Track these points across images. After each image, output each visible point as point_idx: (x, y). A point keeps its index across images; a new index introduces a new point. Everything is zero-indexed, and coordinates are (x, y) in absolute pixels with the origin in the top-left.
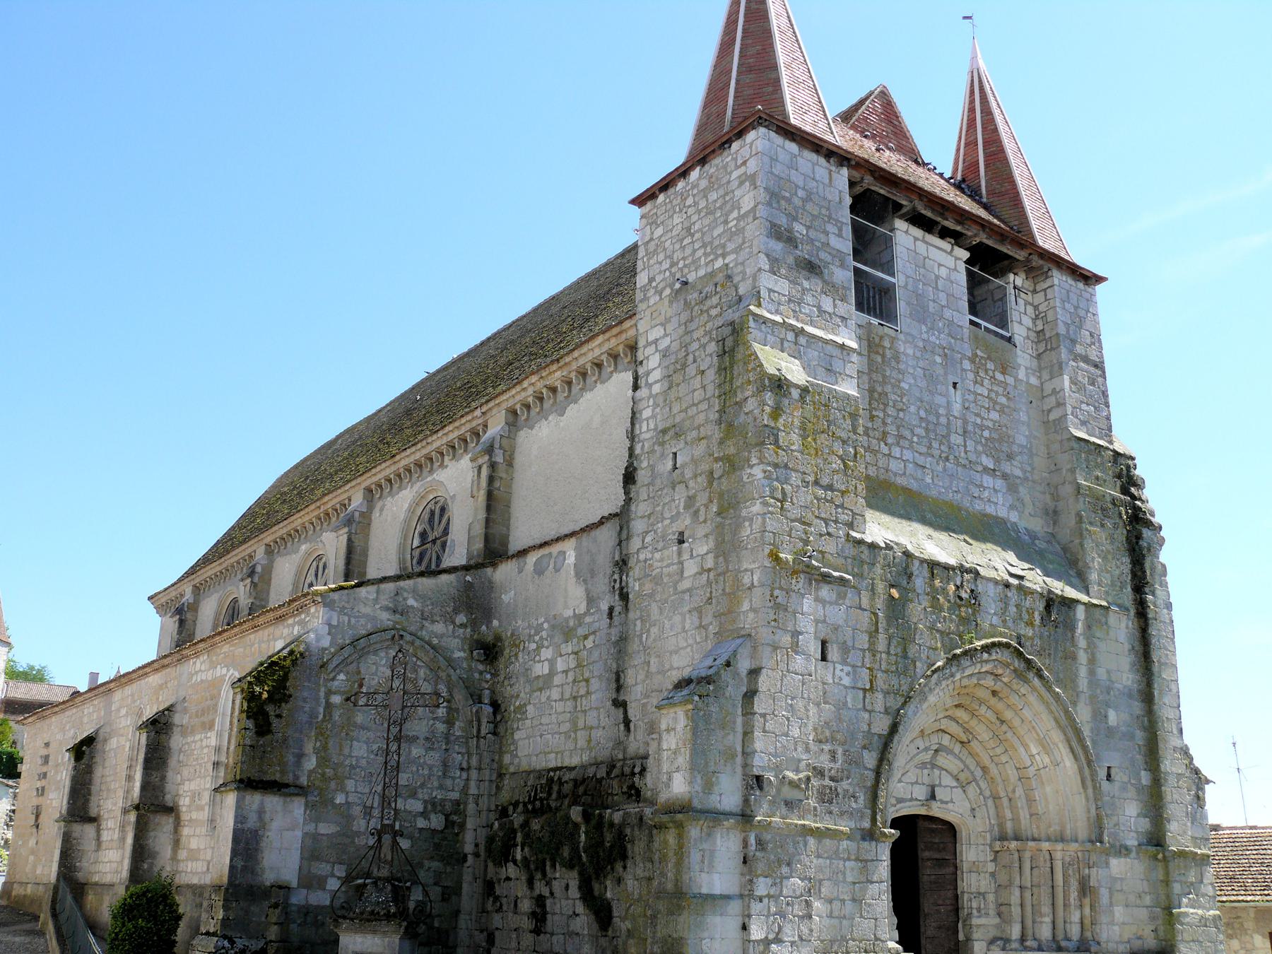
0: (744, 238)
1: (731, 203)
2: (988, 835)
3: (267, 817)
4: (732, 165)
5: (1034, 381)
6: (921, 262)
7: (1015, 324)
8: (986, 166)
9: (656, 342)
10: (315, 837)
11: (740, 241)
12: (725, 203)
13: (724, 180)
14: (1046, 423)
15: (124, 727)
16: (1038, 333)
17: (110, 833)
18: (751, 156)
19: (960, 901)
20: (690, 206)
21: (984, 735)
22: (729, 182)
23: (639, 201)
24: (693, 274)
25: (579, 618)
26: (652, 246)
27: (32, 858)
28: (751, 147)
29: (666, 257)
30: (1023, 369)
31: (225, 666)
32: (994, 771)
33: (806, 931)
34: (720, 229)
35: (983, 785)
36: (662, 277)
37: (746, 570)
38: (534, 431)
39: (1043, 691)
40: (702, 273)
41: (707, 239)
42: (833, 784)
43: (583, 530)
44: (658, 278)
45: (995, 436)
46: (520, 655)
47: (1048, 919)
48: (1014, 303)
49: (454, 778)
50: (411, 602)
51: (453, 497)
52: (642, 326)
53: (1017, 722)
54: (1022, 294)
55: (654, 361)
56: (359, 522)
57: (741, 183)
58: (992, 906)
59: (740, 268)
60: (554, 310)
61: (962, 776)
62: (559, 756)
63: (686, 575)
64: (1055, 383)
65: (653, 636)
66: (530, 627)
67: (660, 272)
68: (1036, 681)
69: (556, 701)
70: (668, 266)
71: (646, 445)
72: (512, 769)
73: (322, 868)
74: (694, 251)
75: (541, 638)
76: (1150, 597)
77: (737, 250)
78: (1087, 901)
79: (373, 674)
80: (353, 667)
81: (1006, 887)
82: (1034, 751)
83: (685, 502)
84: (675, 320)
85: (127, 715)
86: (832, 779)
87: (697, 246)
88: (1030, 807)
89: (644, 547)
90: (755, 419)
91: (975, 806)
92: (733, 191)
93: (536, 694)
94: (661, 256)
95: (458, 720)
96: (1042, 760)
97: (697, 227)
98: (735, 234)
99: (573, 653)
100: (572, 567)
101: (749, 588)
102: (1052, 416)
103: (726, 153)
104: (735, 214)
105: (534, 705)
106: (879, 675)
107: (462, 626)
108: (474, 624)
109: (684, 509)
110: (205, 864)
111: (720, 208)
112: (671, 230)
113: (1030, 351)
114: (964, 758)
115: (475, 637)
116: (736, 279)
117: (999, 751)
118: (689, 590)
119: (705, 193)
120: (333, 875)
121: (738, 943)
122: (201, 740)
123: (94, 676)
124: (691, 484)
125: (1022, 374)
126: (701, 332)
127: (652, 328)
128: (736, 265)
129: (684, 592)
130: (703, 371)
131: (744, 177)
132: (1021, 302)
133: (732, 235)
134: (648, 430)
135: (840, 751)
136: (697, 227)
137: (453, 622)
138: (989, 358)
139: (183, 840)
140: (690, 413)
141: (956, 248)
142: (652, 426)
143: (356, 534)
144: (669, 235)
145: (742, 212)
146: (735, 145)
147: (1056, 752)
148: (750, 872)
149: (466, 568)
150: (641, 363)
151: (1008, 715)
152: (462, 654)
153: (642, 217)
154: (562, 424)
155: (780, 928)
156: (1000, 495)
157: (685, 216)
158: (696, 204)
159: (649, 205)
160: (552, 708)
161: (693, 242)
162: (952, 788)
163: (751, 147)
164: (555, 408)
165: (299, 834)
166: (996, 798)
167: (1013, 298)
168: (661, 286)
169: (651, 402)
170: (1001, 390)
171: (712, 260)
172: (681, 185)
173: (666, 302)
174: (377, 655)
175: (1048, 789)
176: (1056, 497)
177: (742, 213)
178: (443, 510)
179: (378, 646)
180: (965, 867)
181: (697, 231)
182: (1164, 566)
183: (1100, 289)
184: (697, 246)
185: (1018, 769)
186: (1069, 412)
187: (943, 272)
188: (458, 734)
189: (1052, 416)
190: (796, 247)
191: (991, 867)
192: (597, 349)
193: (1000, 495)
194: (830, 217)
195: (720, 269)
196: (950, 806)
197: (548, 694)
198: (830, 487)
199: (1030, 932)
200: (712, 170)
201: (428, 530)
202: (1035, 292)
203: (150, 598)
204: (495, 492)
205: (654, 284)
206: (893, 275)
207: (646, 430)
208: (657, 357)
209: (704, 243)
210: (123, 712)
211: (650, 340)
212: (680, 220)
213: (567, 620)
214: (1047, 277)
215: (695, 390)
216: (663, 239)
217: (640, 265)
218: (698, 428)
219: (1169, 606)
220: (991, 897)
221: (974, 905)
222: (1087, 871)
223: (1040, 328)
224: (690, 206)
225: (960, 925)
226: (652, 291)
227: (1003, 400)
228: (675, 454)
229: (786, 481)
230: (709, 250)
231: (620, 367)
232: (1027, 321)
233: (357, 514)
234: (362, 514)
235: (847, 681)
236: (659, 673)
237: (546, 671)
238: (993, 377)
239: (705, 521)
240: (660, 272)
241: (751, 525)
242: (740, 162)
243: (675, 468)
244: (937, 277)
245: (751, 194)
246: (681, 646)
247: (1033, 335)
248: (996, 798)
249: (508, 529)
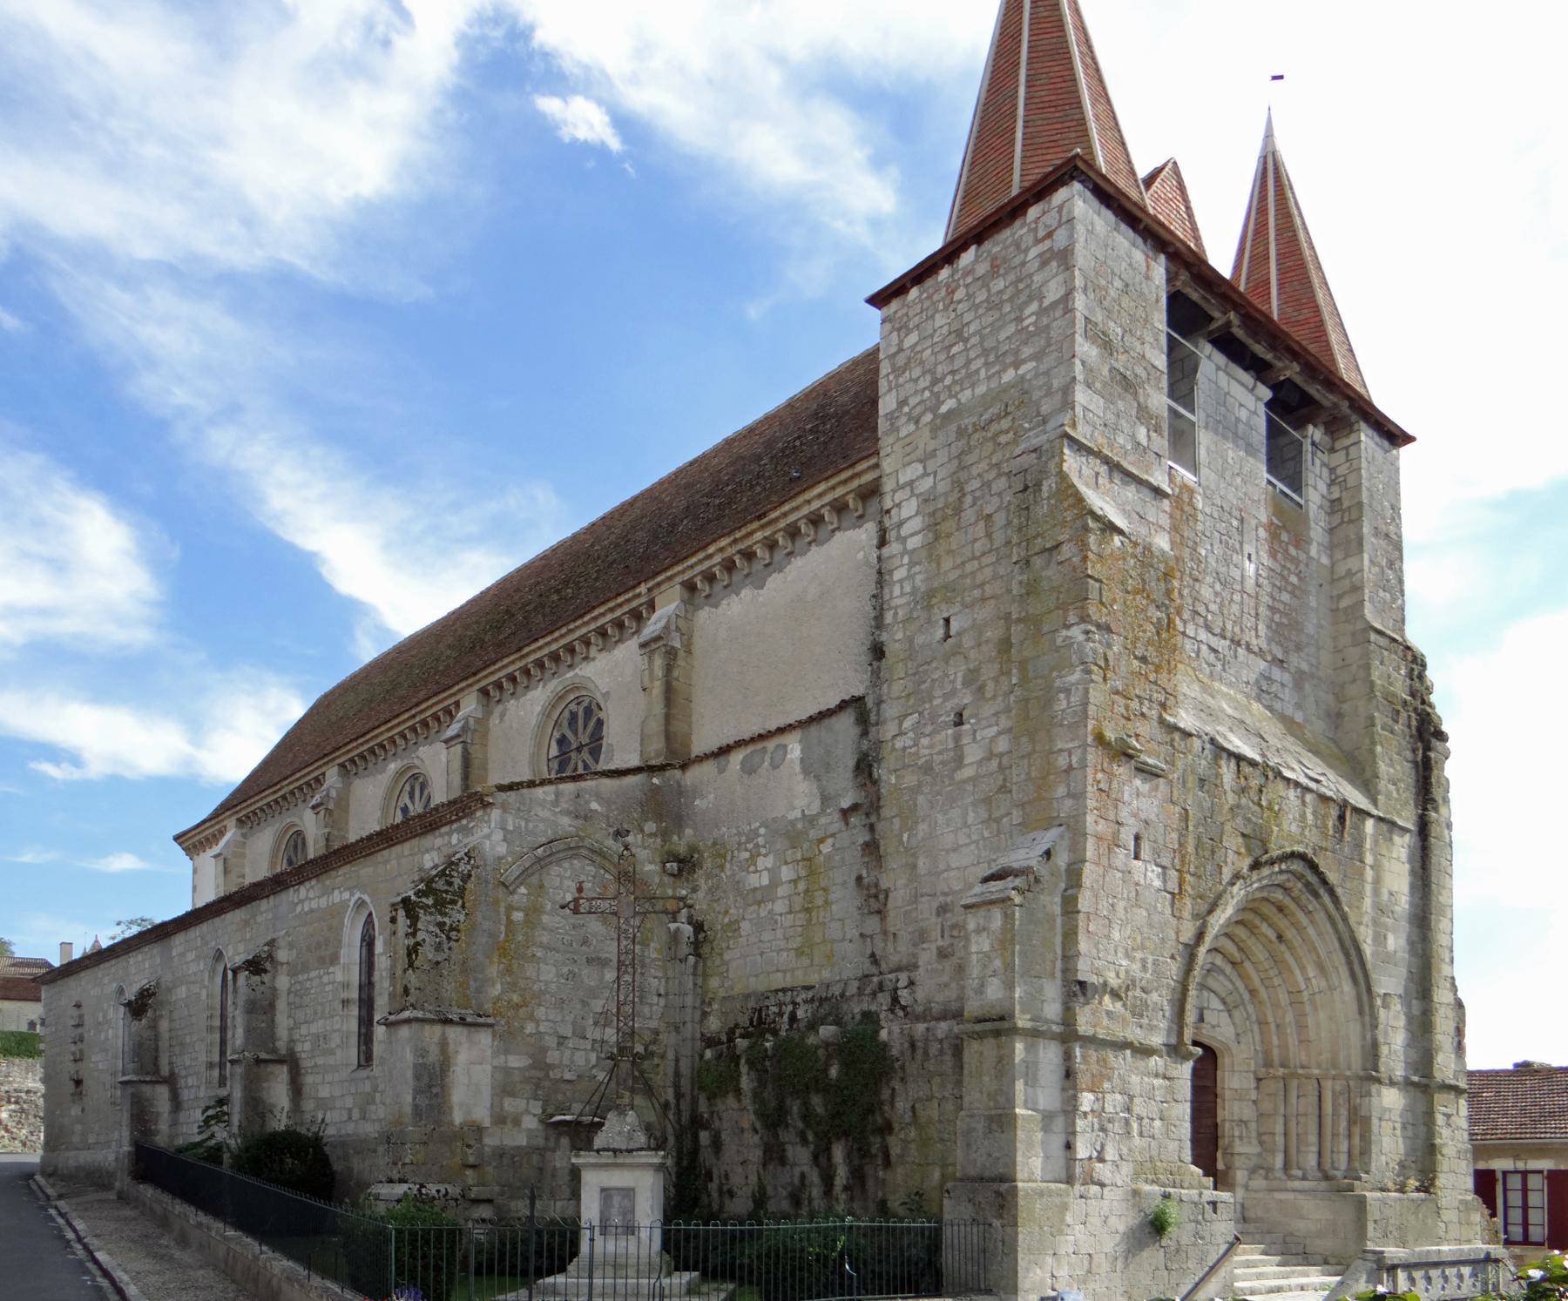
0: (1049, 339)
1: (1027, 292)
2: (1252, 1063)
3: (451, 1048)
4: (1030, 239)
5: (1325, 560)
6: (1223, 399)
7: (1311, 490)
8: (1281, 285)
9: (911, 483)
10: (507, 1071)
11: (1043, 342)
12: (1019, 292)
13: (1017, 261)
14: (1335, 611)
15: (195, 974)
16: (1332, 502)
17: (193, 1091)
18: (1060, 225)
19: (1220, 1130)
20: (960, 302)
21: (1259, 953)
22: (1023, 264)
23: (879, 300)
24: (968, 393)
25: (811, 821)
26: (901, 360)
27: (78, 1128)
28: (1060, 212)
29: (924, 373)
30: (1315, 544)
31: (348, 889)
32: (1263, 994)
33: (1125, 1151)
34: (1011, 329)
35: (1250, 1008)
36: (917, 400)
37: (1061, 750)
38: (720, 610)
39: (1330, 906)
40: (981, 389)
41: (989, 344)
42: (1144, 995)
43: (811, 720)
44: (913, 401)
45: (1285, 621)
46: (728, 865)
47: (1315, 1149)
48: (1310, 463)
49: (651, 1005)
50: (594, 806)
51: (606, 695)
52: (887, 465)
53: (1297, 942)
54: (1319, 453)
55: (909, 509)
56: (475, 731)
57: (1044, 264)
58: (1254, 1134)
59: (1042, 380)
60: (640, 504)
61: (1229, 999)
62: (788, 975)
63: (966, 761)
64: (1352, 564)
65: (921, 834)
66: (739, 834)
67: (916, 392)
68: (1326, 898)
69: (781, 915)
70: (928, 384)
71: (900, 612)
72: (722, 993)
73: (510, 1105)
74: (969, 362)
75: (757, 846)
76: (1433, 814)
77: (1036, 357)
78: (1356, 1130)
79: (556, 888)
80: (534, 880)
81: (1269, 1115)
82: (1311, 975)
83: (964, 678)
84: (942, 457)
85: (198, 958)
86: (1143, 990)
87: (972, 354)
88: (1299, 1034)
89: (901, 734)
90: (1074, 569)
91: (1240, 1031)
92: (1030, 276)
93: (752, 908)
94: (917, 372)
95: (652, 940)
96: (1318, 983)
97: (972, 328)
98: (1034, 334)
99: (804, 859)
100: (798, 762)
101: (1065, 771)
102: (1344, 603)
103: (1018, 223)
104: (1034, 307)
105: (750, 920)
106: (1188, 877)
107: (650, 835)
108: (665, 835)
109: (963, 684)
110: (345, 1113)
111: (1010, 300)
112: (932, 336)
113: (1322, 524)
115: (666, 848)
116: (1036, 395)
117: (1272, 973)
118: (970, 779)
119: (984, 281)
120: (527, 1112)
121: (1062, 1162)
122: (321, 977)
123: (66, 946)
124: (973, 654)
125: (1313, 552)
126: (984, 465)
127: (904, 466)
128: (1036, 376)
129: (965, 781)
130: (989, 516)
131: (1048, 255)
132: (1317, 462)
133: (1025, 336)
134: (902, 594)
135: (1150, 959)
136: (972, 328)
137: (642, 831)
138: (1284, 527)
139: (307, 1090)
140: (969, 568)
141: (1259, 385)
142: (908, 589)
143: (472, 744)
144: (928, 343)
145: (1046, 303)
146: (1033, 212)
147: (1334, 976)
148: (1075, 1087)
149: (647, 769)
150: (888, 511)
151: (1290, 934)
152: (652, 867)
153: (884, 321)
154: (761, 599)
155: (1103, 1146)
156: (1287, 690)
157: (953, 315)
158: (970, 296)
159: (895, 305)
160: (776, 922)
161: (966, 350)
163: (1060, 212)
164: (747, 582)
165: (488, 1068)
166: (1262, 1023)
167: (1310, 455)
168: (918, 410)
169: (906, 560)
170: (1293, 568)
171: (999, 372)
172: (944, 273)
173: (926, 432)
174: (560, 866)
175: (1322, 1015)
176: (1340, 698)
177: (1044, 305)
178: (588, 712)
179: (561, 855)
180: (1228, 1094)
181: (974, 334)
182: (1447, 780)
183: (1405, 452)
184: (972, 354)
185: (1289, 992)
186: (1366, 598)
187: (1243, 415)
188: (654, 956)
189: (1344, 603)
190: (1111, 355)
192: (817, 498)
193: (1287, 690)
194: (1146, 321)
195: (1011, 385)
196: (1217, 1029)
197: (770, 907)
199: (1294, 1158)
200: (996, 249)
201: (569, 735)
202: (1332, 450)
203: (176, 838)
204: (674, 683)
205: (906, 409)
206: (1193, 412)
207: (897, 596)
208: (914, 503)
209: (984, 350)
210: (191, 956)
211: (901, 482)
212: (945, 321)
213: (793, 823)
214: (1352, 431)
215: (975, 540)
216: (919, 348)
217: (883, 385)
218: (982, 585)
219: (1449, 826)
220: (1253, 1126)
221: (1237, 1133)
222: (1358, 1100)
223: (1336, 495)
224: (960, 302)
225: (1219, 1155)
226: (904, 419)
227: (1294, 579)
228: (947, 621)
229: (1109, 646)
230: (992, 358)
231: (844, 524)
232: (1322, 487)
233: (471, 721)
234: (477, 720)
235: (1157, 883)
236: (930, 874)
237: (765, 881)
238: (1286, 551)
239: (994, 697)
240: (916, 392)
241: (1068, 697)
242: (1041, 234)
243: (947, 636)
244: (1238, 420)
245: (1060, 278)
246: (961, 843)
247: (1327, 504)
248: (1262, 1023)
249: (690, 727)
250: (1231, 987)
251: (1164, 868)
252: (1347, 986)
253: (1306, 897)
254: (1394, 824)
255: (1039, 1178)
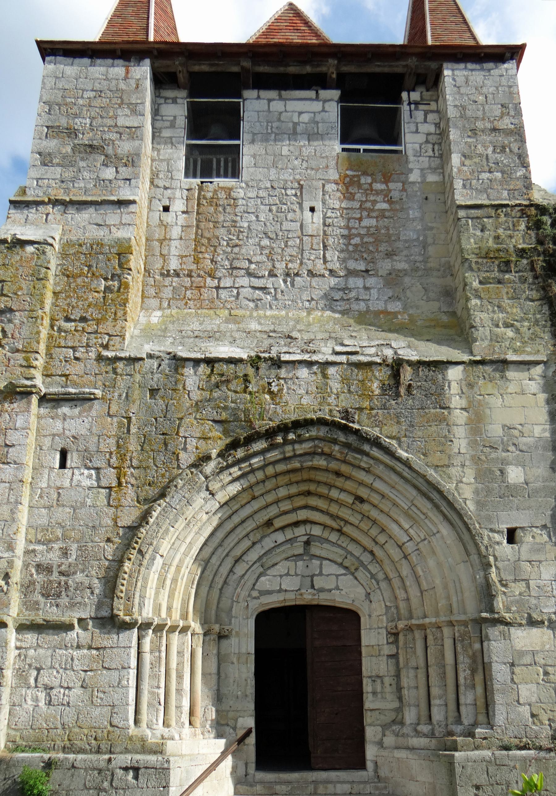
2: (384, 618)
68: (376, 452)
82: (406, 526)
114: (344, 545)
151: (363, 492)
162: (337, 576)
191: (387, 650)
198: (83, 319)
250: (342, 552)
251: (97, 469)
252: (445, 530)
253: (351, 456)
254: (505, 362)
255: (430, 727)
